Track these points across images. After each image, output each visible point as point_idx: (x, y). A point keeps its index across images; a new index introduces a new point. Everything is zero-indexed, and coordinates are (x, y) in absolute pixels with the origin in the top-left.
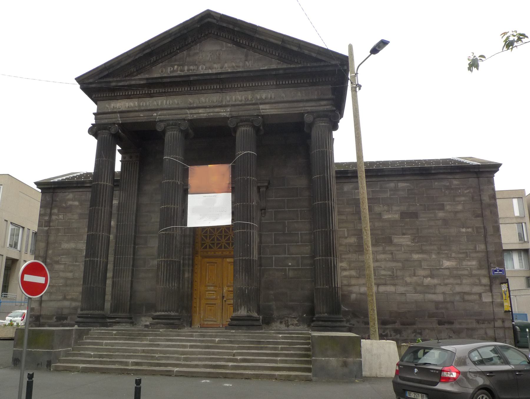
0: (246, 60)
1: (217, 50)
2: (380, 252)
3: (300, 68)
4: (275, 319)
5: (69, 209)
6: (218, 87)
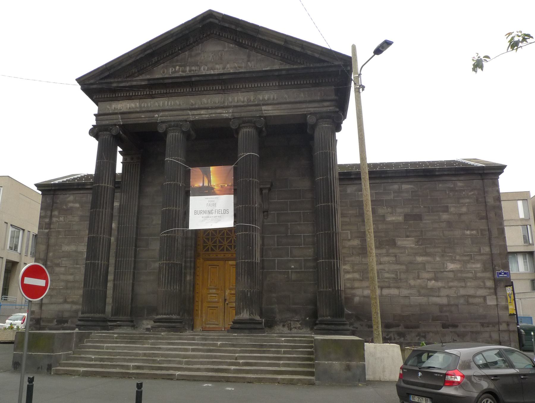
0: (248, 61)
1: (220, 51)
2: (384, 254)
3: (303, 68)
4: (278, 323)
5: (69, 211)
6: (220, 88)
